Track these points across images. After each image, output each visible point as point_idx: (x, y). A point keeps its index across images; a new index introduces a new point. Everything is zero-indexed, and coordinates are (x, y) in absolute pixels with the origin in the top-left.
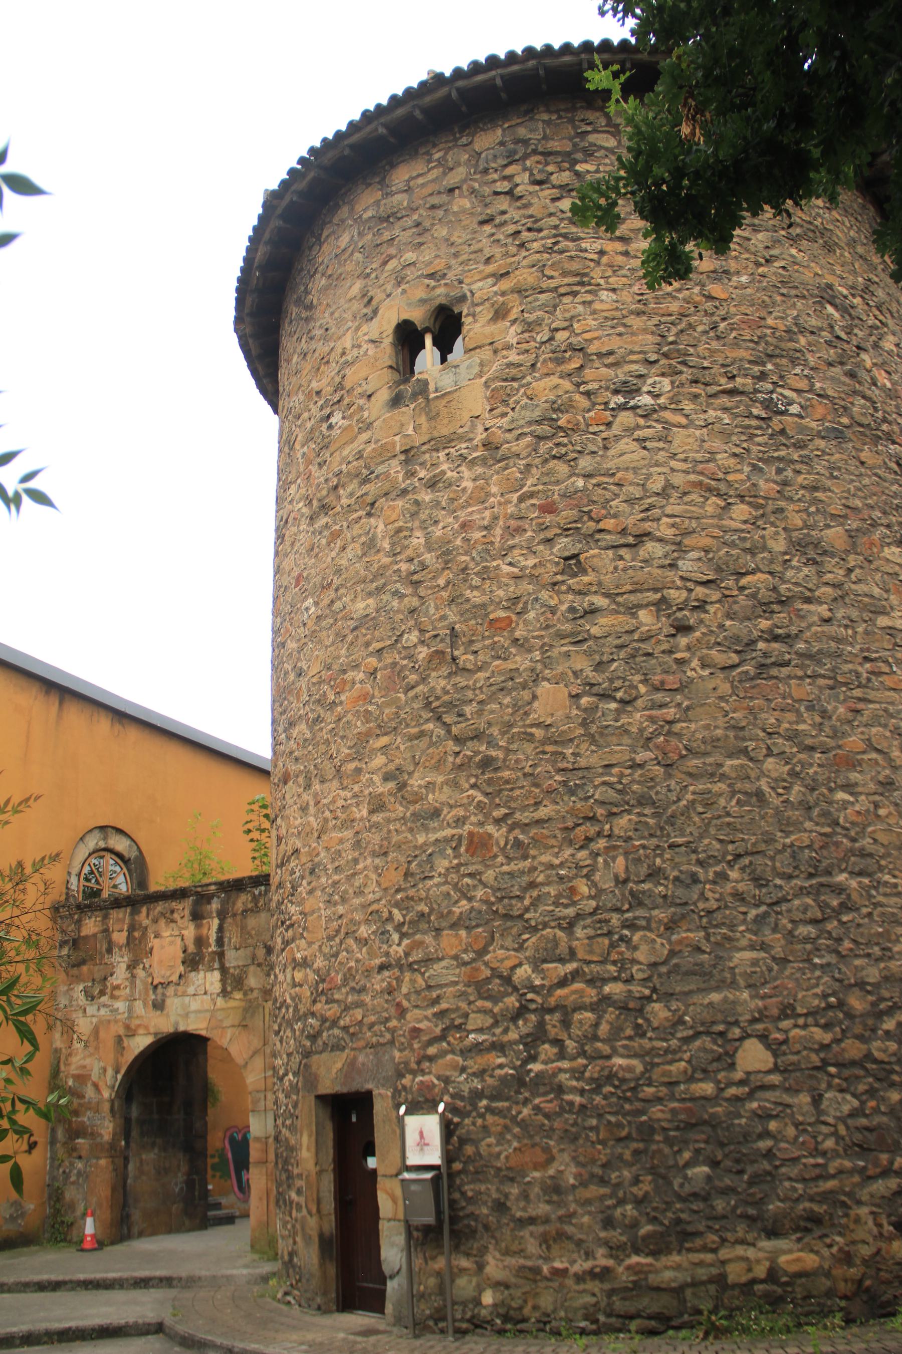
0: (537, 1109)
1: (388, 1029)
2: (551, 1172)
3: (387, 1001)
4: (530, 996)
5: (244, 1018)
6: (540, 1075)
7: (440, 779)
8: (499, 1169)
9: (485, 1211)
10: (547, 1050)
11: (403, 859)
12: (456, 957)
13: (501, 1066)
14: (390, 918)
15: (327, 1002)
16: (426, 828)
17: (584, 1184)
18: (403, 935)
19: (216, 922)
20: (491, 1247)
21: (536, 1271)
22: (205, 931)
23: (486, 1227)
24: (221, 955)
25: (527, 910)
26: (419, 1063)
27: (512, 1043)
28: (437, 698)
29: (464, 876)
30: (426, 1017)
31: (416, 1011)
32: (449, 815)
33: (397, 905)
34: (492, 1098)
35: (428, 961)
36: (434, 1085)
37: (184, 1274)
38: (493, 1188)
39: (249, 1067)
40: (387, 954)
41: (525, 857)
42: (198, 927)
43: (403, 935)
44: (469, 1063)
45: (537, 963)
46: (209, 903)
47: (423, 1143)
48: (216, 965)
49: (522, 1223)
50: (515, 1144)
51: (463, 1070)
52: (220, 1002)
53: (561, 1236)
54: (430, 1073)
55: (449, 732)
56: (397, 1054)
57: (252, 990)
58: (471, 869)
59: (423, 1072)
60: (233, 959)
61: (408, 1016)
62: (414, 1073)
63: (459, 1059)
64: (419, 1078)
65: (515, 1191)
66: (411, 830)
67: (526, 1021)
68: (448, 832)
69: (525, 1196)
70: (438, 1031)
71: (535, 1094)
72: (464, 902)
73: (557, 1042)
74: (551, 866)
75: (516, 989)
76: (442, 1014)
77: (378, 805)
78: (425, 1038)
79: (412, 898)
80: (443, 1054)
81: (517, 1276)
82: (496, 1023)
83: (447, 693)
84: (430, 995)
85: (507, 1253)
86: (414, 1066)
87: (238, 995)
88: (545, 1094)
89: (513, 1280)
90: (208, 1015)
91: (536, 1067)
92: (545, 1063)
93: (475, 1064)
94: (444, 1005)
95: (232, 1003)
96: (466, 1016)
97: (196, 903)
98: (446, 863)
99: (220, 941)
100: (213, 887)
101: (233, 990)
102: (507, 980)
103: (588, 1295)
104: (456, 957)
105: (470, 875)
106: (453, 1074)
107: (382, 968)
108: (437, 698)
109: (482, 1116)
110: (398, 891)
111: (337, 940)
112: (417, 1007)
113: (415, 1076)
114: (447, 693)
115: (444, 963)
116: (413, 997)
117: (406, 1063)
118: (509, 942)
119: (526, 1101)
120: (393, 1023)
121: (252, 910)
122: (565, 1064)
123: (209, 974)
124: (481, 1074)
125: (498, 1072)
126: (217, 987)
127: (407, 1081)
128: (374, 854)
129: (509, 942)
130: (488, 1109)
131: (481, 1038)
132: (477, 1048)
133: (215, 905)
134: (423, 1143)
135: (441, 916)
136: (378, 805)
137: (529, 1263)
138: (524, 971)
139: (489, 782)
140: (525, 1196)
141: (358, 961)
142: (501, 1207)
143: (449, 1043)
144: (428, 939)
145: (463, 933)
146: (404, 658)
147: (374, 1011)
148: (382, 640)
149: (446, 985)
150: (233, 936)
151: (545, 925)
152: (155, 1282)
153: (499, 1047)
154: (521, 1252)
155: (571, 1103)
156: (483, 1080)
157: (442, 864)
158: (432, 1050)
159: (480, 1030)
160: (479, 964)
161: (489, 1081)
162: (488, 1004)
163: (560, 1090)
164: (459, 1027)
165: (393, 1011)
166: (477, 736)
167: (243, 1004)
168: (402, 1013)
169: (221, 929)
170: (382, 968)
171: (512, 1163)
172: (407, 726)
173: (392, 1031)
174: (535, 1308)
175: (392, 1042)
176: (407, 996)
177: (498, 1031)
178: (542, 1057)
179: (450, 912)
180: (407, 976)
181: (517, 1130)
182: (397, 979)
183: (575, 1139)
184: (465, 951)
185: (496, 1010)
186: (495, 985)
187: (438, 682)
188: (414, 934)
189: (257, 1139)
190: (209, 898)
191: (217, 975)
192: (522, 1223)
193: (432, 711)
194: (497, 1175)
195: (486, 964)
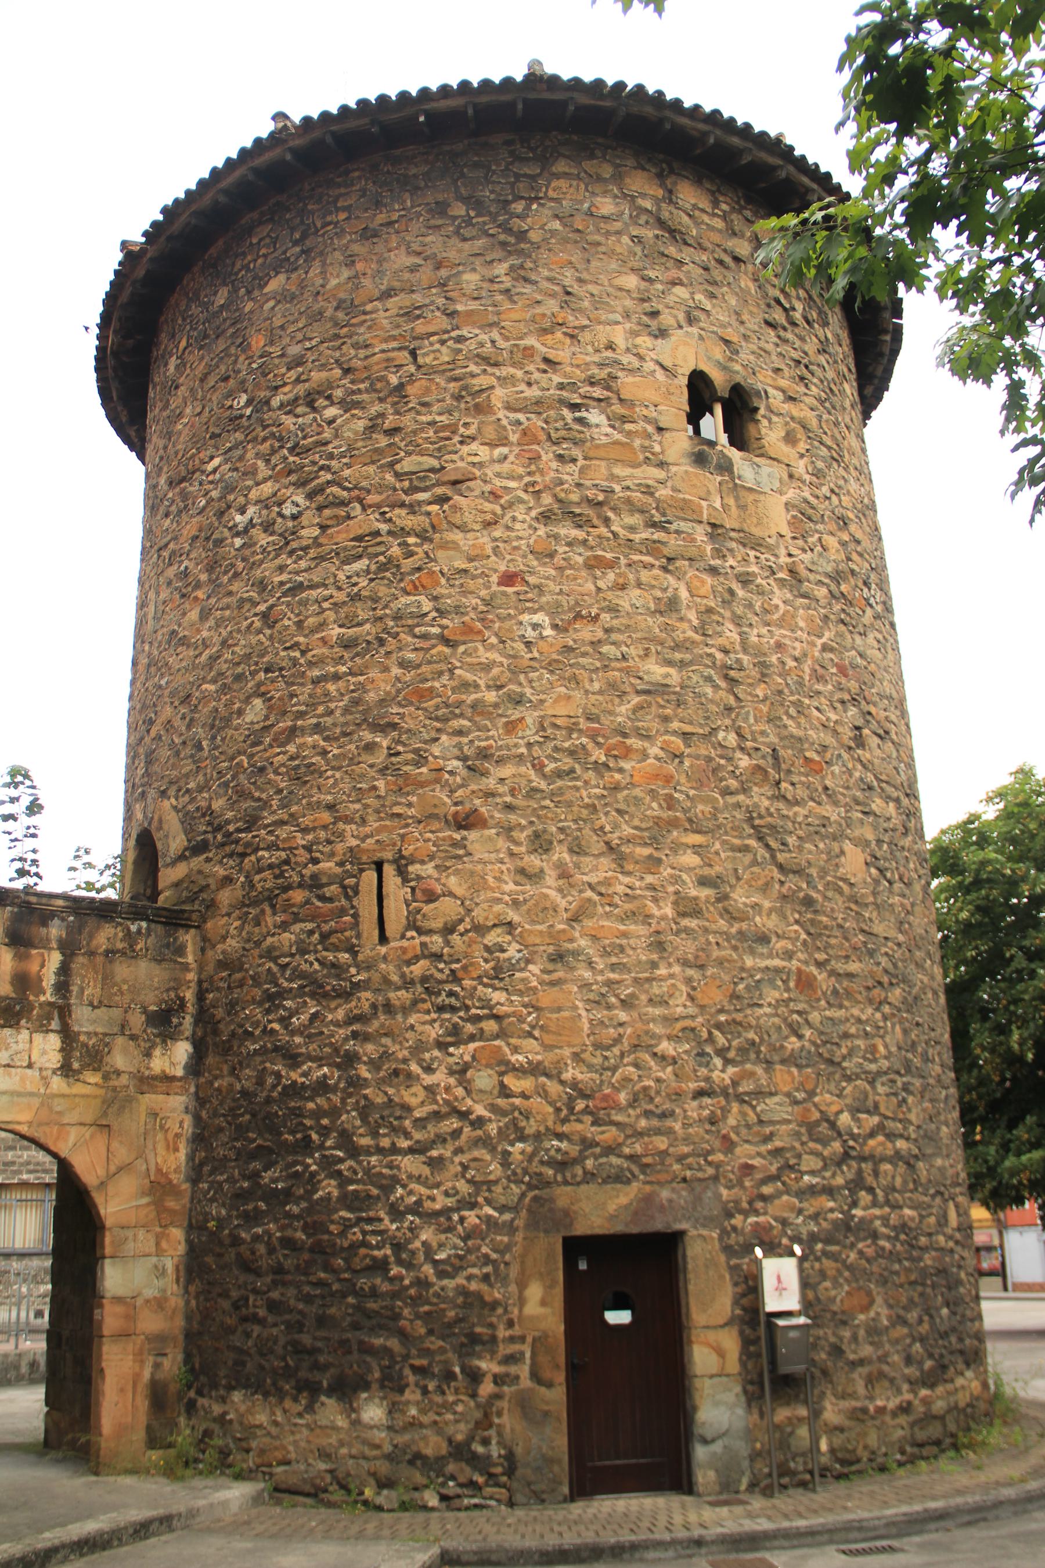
0: (861, 1253)
1: (710, 1164)
2: (872, 1314)
3: (707, 1132)
4: (851, 1143)
5: (105, 1114)
6: (862, 1220)
7: (767, 904)
8: (835, 1313)
9: (823, 1356)
10: (864, 1197)
11: (727, 978)
12: (788, 1095)
13: (832, 1210)
14: (711, 1039)
15: (593, 1124)
16: (752, 952)
17: (893, 1325)
18: (727, 1062)
19: (55, 958)
20: (828, 1392)
21: (864, 1410)
22: (34, 967)
23: (825, 1372)
24: (64, 1011)
25: (844, 1058)
26: (750, 1203)
27: (840, 1188)
28: (760, 817)
29: (793, 1012)
30: (759, 1154)
31: (747, 1146)
32: (780, 945)
33: (719, 1026)
34: (827, 1241)
35: (760, 1094)
36: (772, 1227)
37: (182, 1509)
38: (829, 1332)
39: (111, 1190)
40: (707, 1079)
41: (841, 1006)
42: (19, 957)
43: (727, 1062)
44: (805, 1205)
45: (854, 1111)
46: (44, 923)
47: (780, 1289)
48: (55, 1025)
49: (854, 1364)
50: (846, 1288)
51: (800, 1212)
52: (58, 1083)
53: (882, 1375)
54: (765, 1213)
55: (773, 857)
56: (724, 1192)
57: (118, 1073)
58: (800, 1007)
59: (757, 1213)
60: (85, 1020)
61: (738, 1150)
62: (746, 1214)
63: (795, 1200)
64: (752, 1219)
65: (847, 1334)
66: (735, 948)
67: (849, 1167)
68: (777, 962)
69: (855, 1338)
70: (773, 1169)
71: (859, 1239)
72: (793, 1039)
73: (871, 1190)
74: (859, 1021)
75: (840, 1134)
76: (777, 1152)
77: (687, 908)
78: (759, 1176)
79: (740, 1024)
80: (778, 1194)
81: (850, 1418)
82: (825, 1167)
83: (771, 815)
84: (762, 1130)
85: (844, 1396)
86: (745, 1205)
87: (93, 1078)
88: (865, 1239)
89: (847, 1423)
90: (36, 1102)
91: (858, 1212)
92: (865, 1209)
93: (811, 1206)
94: (778, 1143)
95: (79, 1089)
96: (799, 1156)
97: (16, 919)
98: (777, 995)
99: (62, 987)
100: (60, 902)
101: (83, 1068)
102: (833, 1125)
103: (899, 1430)
104: (788, 1095)
105: (799, 1013)
106: (791, 1216)
107: (700, 1094)
108: (760, 817)
109: (817, 1259)
110: (721, 1011)
111: (616, 1051)
112: (747, 1141)
113: (746, 1217)
114: (771, 815)
115: (776, 1099)
116: (744, 1131)
117: (737, 1202)
118: (832, 1087)
119: (853, 1246)
120: (719, 1157)
121: (124, 954)
122: (877, 1212)
123: (38, 1038)
124: (815, 1217)
125: (830, 1216)
126: (54, 1059)
127: (737, 1220)
128: (685, 963)
129: (832, 1087)
130: (825, 1253)
131: (815, 1180)
132: (812, 1191)
133: (55, 930)
134: (780, 1289)
135: (773, 1049)
136: (687, 908)
137: (858, 1404)
138: (845, 1118)
139: (812, 922)
140: (855, 1338)
141: (658, 1080)
142: (837, 1351)
143: (784, 1183)
144: (759, 1070)
145: (794, 1070)
146: (721, 757)
147: (687, 1140)
148: (691, 723)
149: (779, 1122)
150: (87, 985)
151: (858, 1077)
152: (155, 1526)
153: (829, 1191)
154: (853, 1396)
155: (883, 1249)
156: (818, 1224)
157: (772, 995)
158: (767, 1190)
159: (812, 1173)
160: (810, 1105)
161: (825, 1225)
162: (819, 1147)
163: (875, 1235)
164: (791, 1168)
165: (717, 1144)
166: (798, 872)
167: (101, 1092)
168: (728, 1145)
169: (64, 970)
170: (700, 1094)
171: (846, 1307)
172: (726, 833)
173: (717, 1166)
174: (866, 1447)
175: (715, 1178)
176: (736, 1129)
177: (828, 1174)
178: (862, 1203)
179: (782, 1047)
180: (735, 1107)
181: (847, 1274)
182: (722, 1108)
183: (885, 1282)
184: (797, 1090)
185: (826, 1153)
186: (824, 1128)
187: (760, 797)
188: (742, 1062)
189: (118, 1300)
190: (45, 918)
191: (54, 1041)
192: (854, 1364)
193: (753, 827)
194: (832, 1320)
195: (816, 1105)
